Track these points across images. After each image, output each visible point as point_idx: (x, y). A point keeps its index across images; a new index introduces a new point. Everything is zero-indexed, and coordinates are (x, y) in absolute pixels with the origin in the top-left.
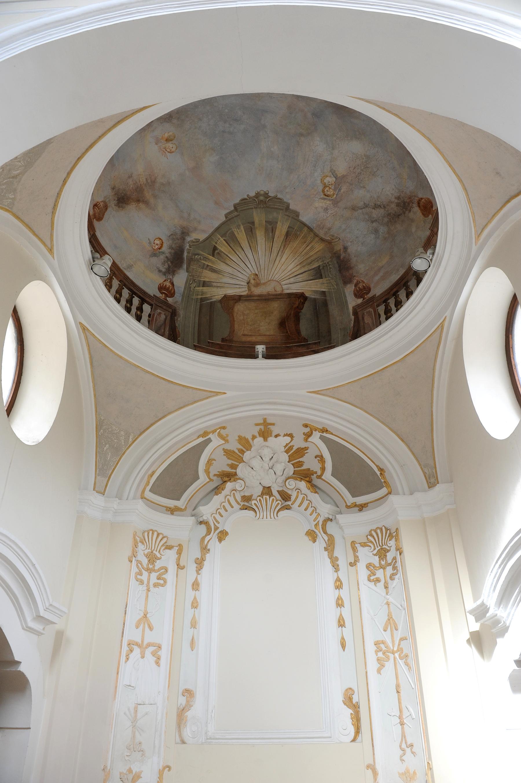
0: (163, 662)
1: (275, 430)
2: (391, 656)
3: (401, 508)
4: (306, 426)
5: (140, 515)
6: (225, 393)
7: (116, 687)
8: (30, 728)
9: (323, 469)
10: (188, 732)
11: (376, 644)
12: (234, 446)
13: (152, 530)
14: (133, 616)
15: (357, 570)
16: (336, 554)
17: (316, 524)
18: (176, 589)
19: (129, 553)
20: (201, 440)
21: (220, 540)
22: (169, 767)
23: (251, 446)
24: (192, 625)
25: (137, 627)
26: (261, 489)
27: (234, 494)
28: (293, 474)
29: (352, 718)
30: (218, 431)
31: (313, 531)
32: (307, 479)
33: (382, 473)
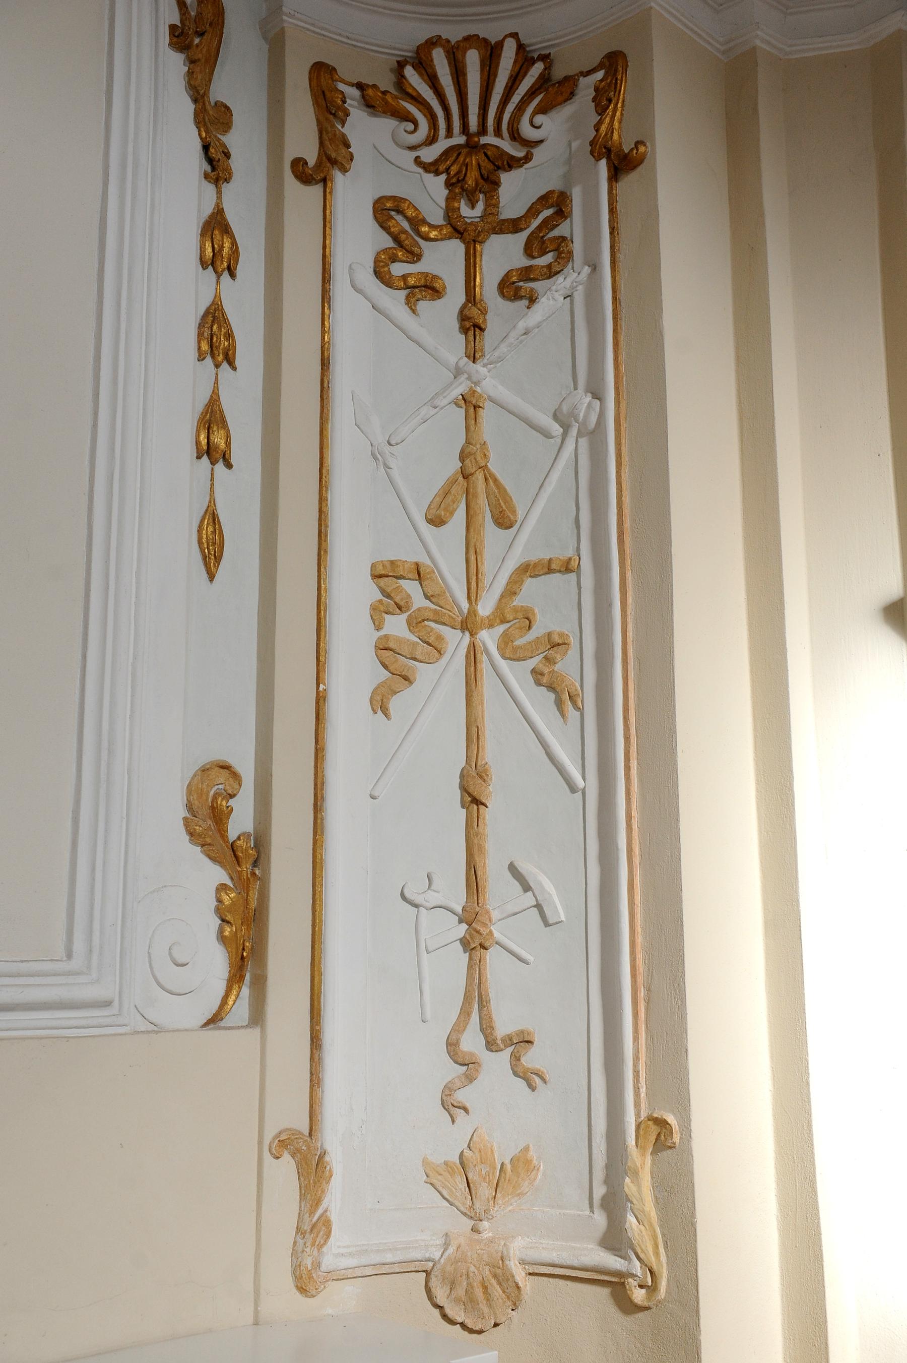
2: (456, 642)
11: (383, 574)
16: (222, 89)
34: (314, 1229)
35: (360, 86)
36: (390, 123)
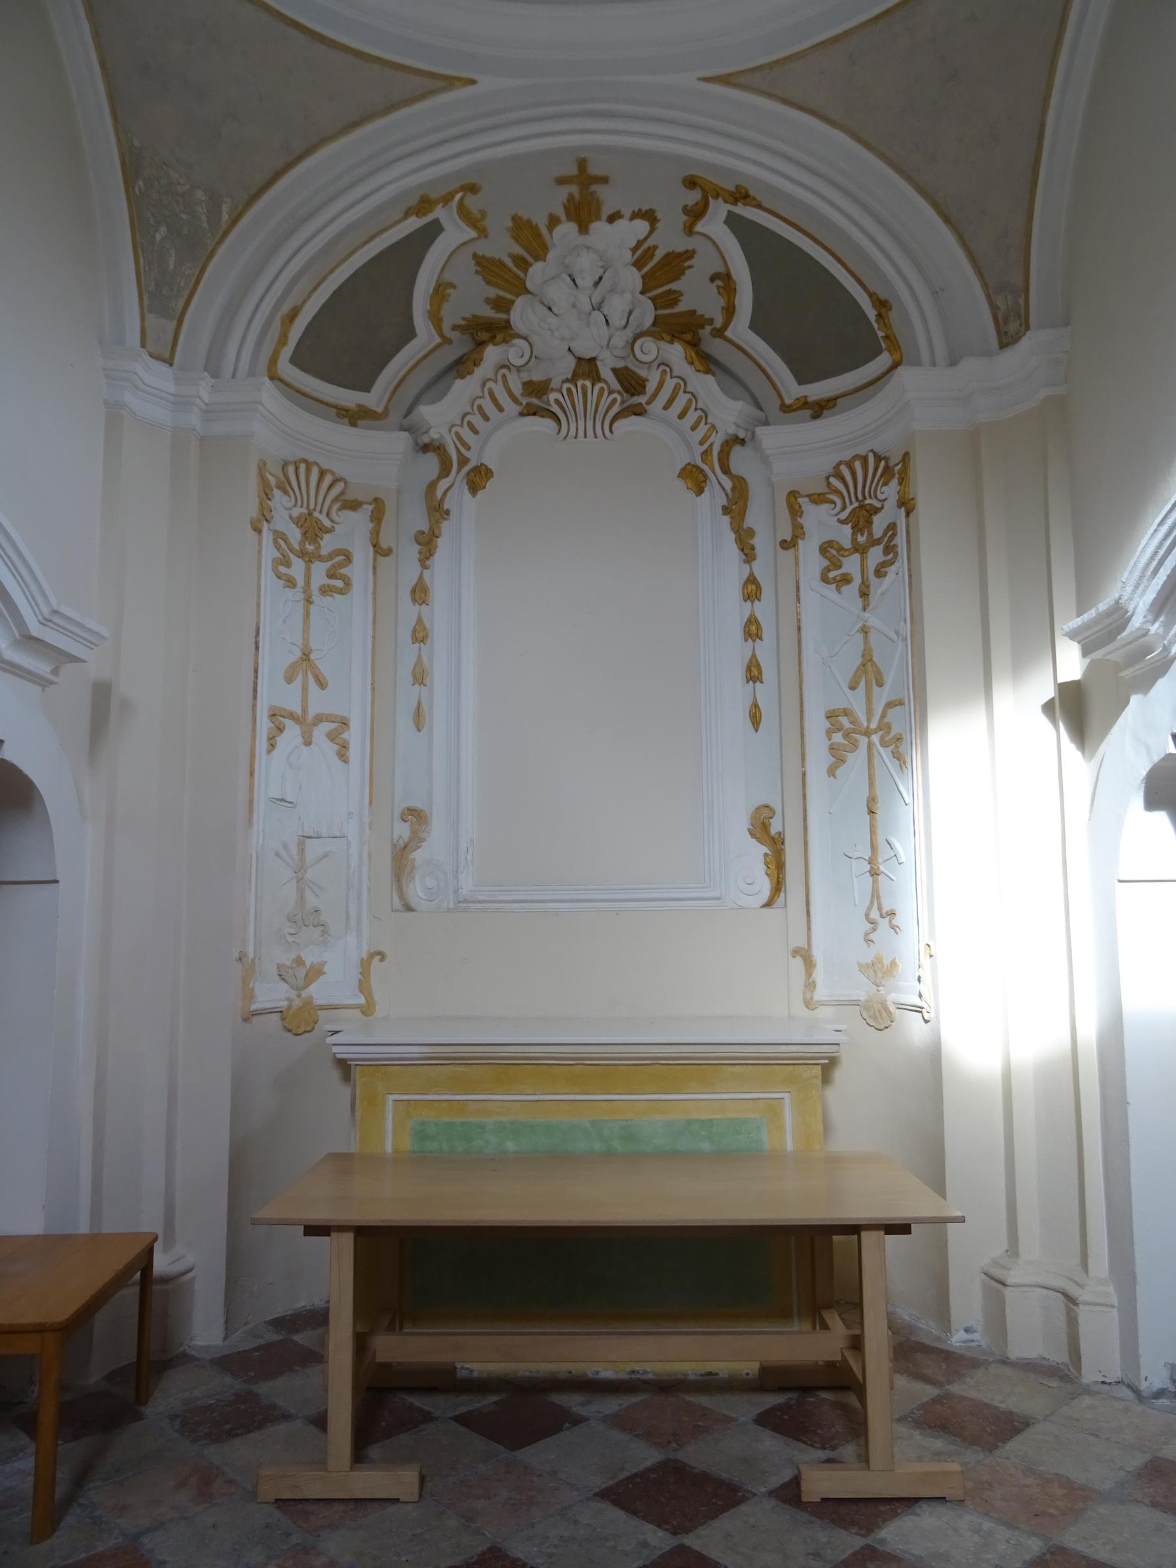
0: (354, 752)
1: (610, 198)
2: (863, 741)
3: (916, 402)
4: (691, 183)
5: (275, 421)
6: (473, 82)
7: (251, 802)
8: (57, 882)
9: (730, 311)
10: (417, 890)
11: (831, 716)
12: (502, 247)
13: (305, 461)
14: (276, 656)
15: (797, 558)
16: (749, 522)
17: (706, 451)
18: (374, 599)
19: (253, 511)
20: (414, 223)
21: (474, 489)
22: (382, 956)
23: (545, 249)
24: (414, 677)
25: (289, 680)
26: (571, 363)
27: (504, 376)
28: (654, 324)
29: (766, 864)
30: (458, 196)
31: (698, 468)
32: (688, 337)
33: (883, 311)
34: (811, 985)
35: (808, 496)
36: (826, 506)
